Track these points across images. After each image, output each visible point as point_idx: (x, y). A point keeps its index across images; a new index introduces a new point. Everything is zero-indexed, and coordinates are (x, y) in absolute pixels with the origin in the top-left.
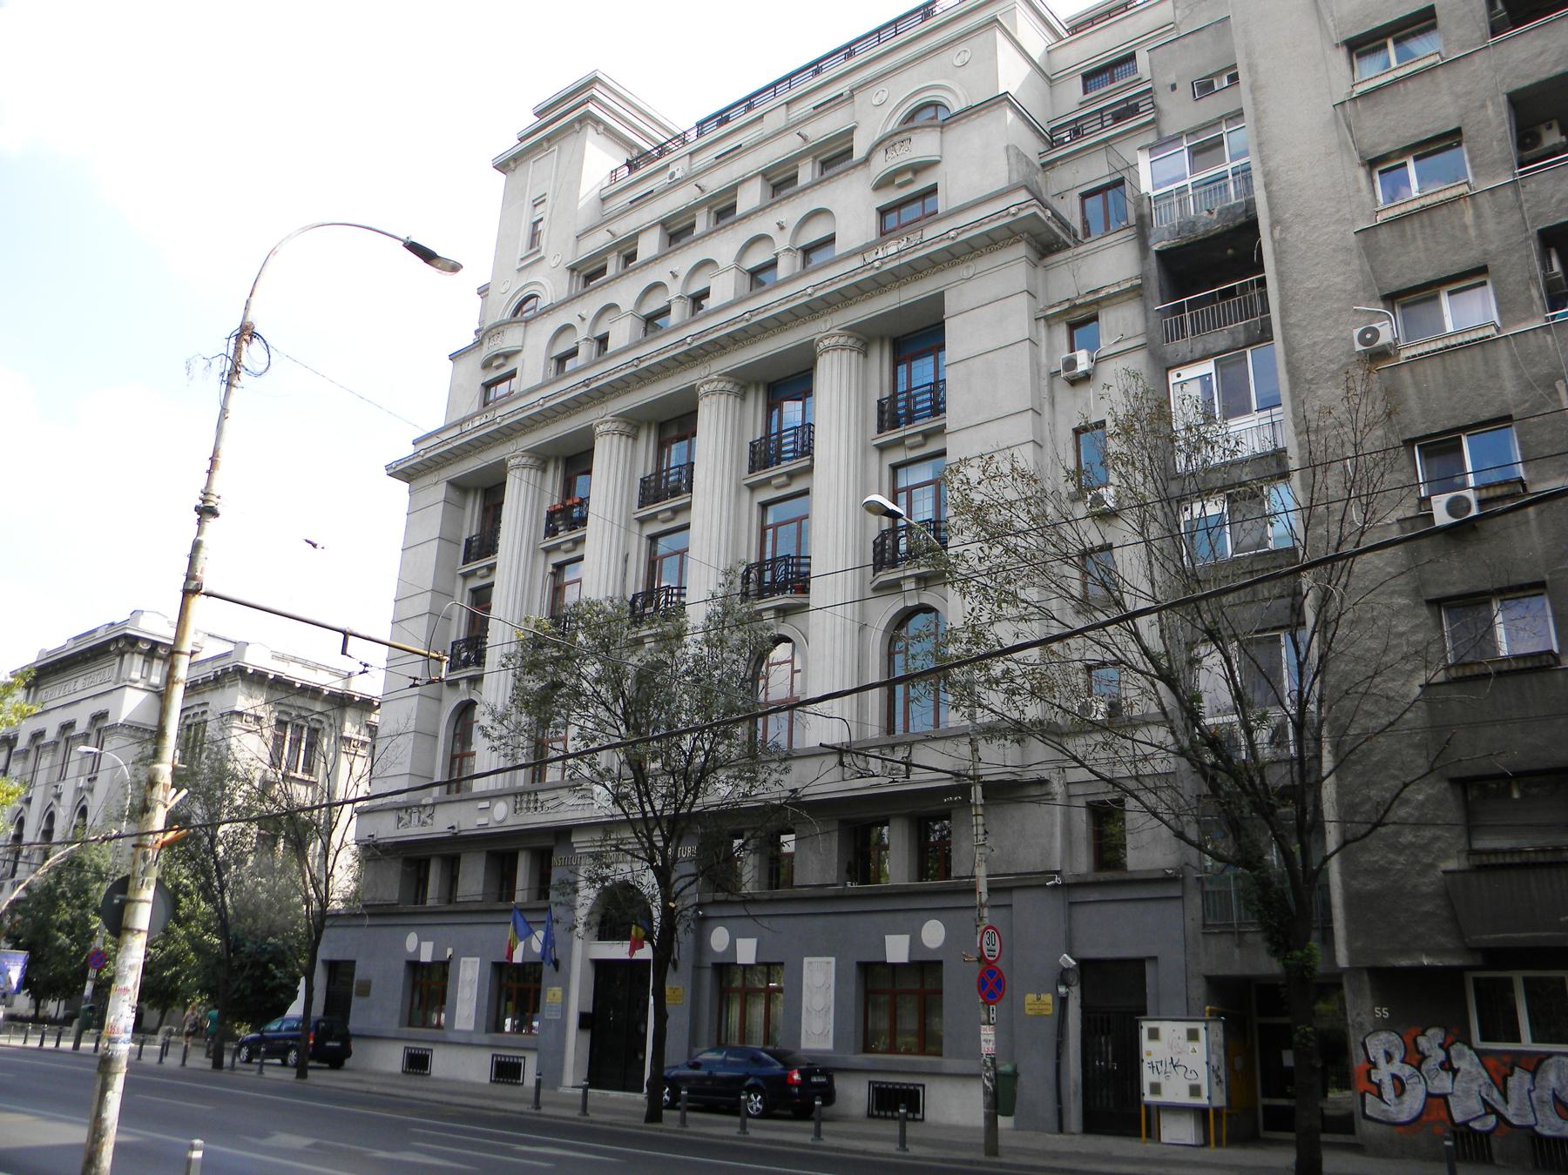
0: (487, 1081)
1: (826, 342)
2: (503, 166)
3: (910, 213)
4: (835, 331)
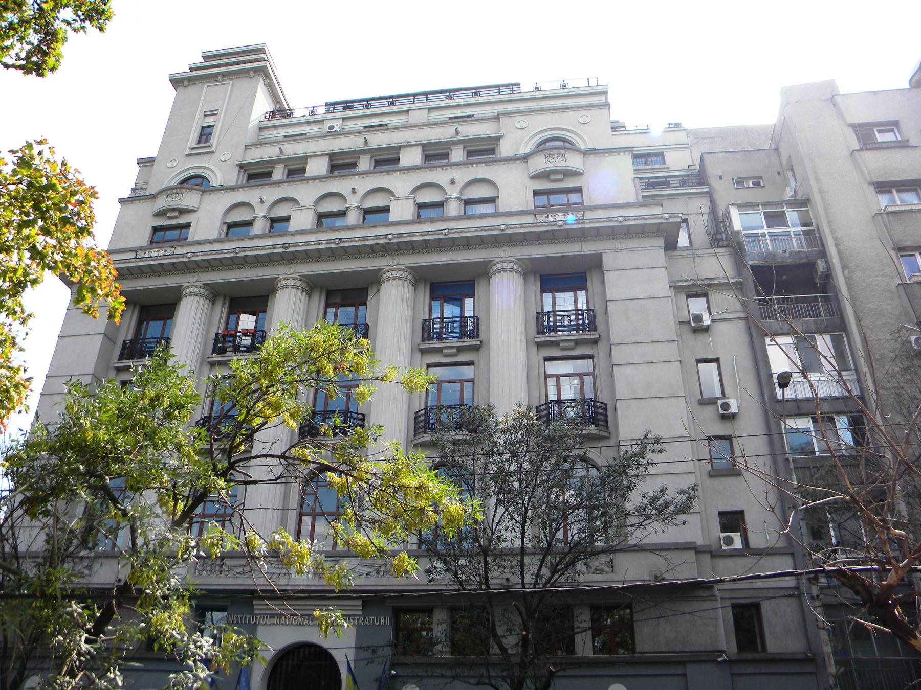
1: (191, 289)
2: (177, 82)
3: (170, 234)
4: (512, 259)
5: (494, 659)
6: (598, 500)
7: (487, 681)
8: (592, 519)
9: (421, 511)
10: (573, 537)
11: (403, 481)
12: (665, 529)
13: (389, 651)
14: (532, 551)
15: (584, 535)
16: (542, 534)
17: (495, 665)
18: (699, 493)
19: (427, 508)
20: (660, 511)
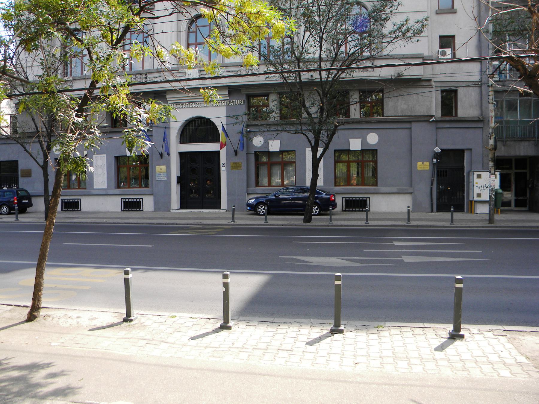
0: (120, 210)
5: (304, 121)
6: (366, 27)
7: (300, 132)
8: (362, 39)
9: (259, 27)
10: (350, 50)
11: (247, 10)
12: (406, 44)
13: (245, 118)
14: (326, 59)
15: (357, 48)
16: (332, 48)
17: (305, 124)
18: (429, 22)
19: (262, 25)
20: (404, 34)
